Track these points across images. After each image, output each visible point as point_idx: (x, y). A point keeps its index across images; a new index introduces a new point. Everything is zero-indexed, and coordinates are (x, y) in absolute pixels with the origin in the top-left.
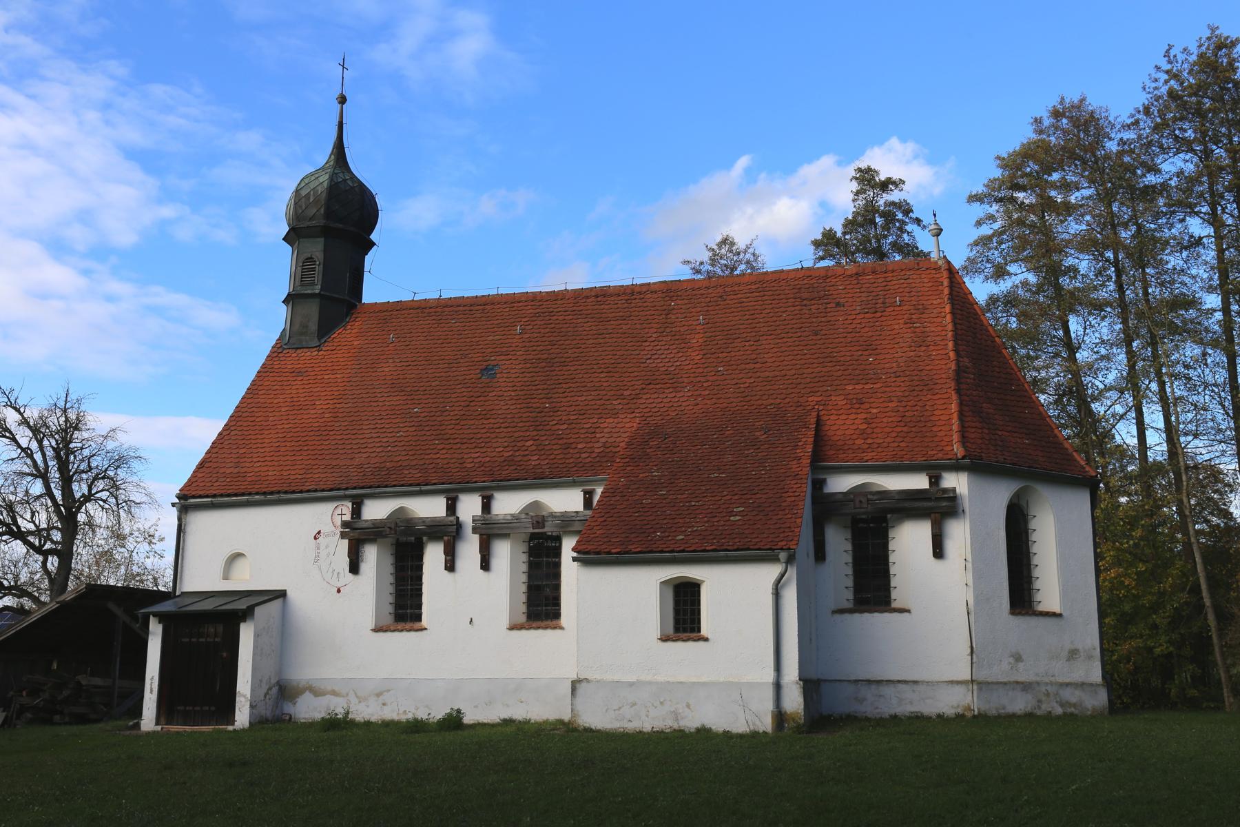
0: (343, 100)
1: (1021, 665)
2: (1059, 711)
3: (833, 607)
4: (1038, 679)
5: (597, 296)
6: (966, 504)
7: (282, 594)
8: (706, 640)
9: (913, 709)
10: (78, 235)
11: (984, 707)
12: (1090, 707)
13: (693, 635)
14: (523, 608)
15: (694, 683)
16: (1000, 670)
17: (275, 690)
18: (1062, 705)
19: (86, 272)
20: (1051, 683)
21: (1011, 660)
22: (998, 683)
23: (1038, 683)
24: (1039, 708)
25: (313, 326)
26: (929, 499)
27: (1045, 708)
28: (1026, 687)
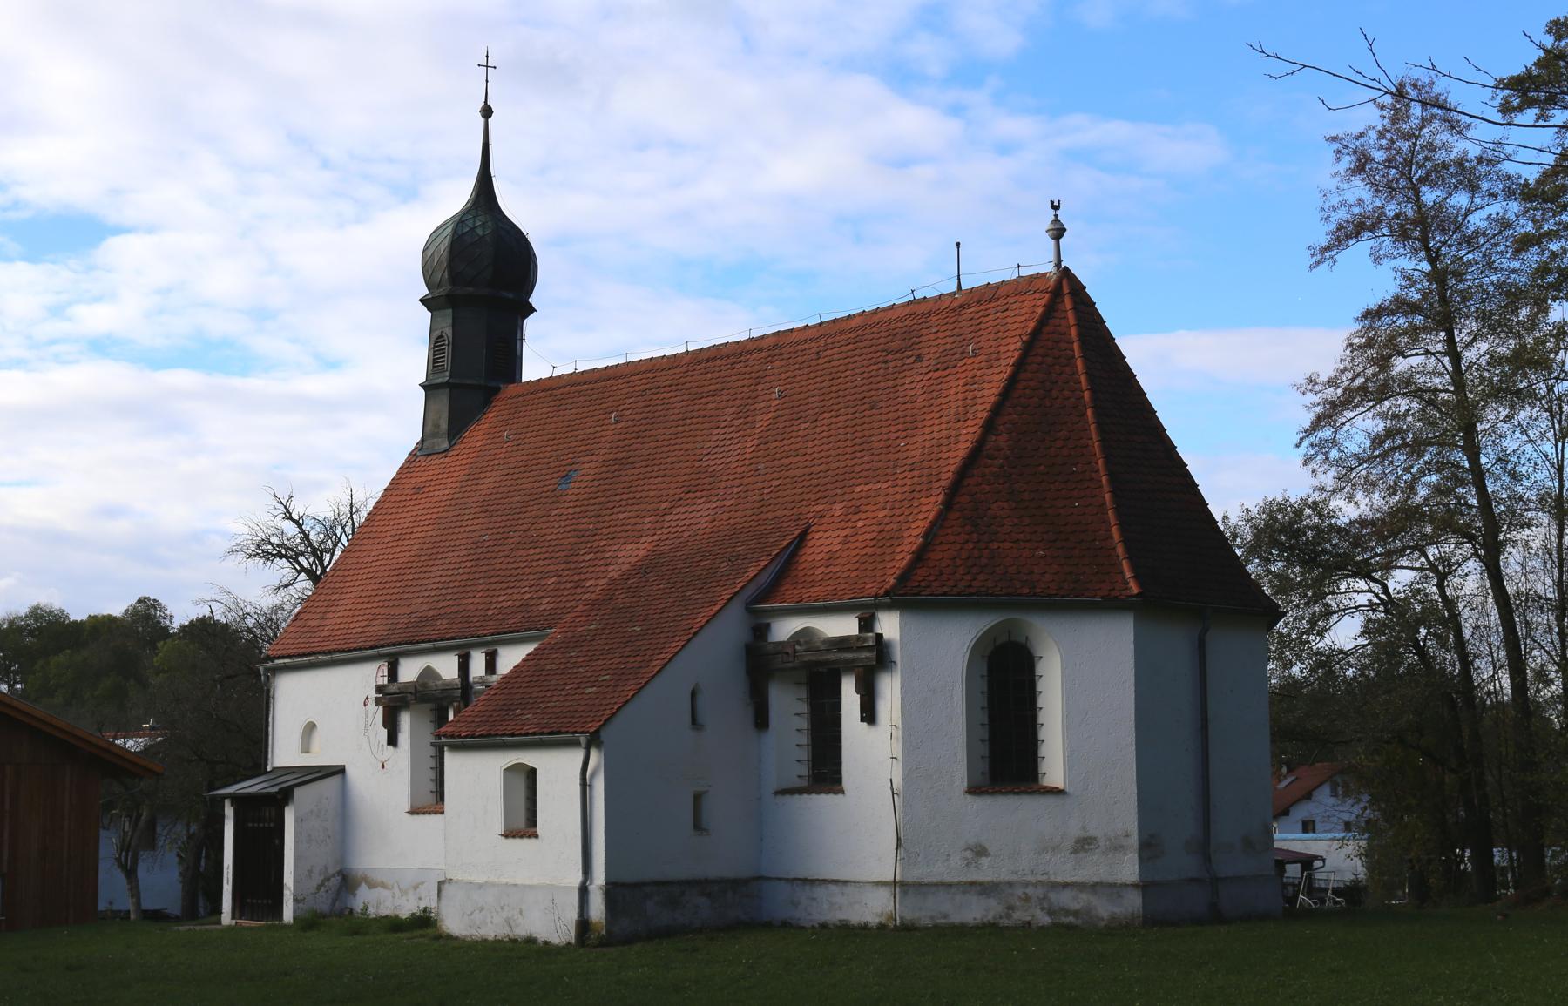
0: (487, 112)
1: (985, 861)
2: (1045, 920)
4: (1014, 878)
5: (708, 360)
6: (897, 655)
7: (340, 771)
10: (928, 51)
11: (909, 916)
15: (525, 886)
16: (950, 868)
17: (335, 881)
18: (1051, 913)
19: (956, 110)
20: (1035, 885)
21: (968, 854)
22: (936, 885)
23: (1010, 884)
24: (1009, 916)
25: (444, 426)
26: (849, 649)
27: (1020, 916)
28: (986, 889)
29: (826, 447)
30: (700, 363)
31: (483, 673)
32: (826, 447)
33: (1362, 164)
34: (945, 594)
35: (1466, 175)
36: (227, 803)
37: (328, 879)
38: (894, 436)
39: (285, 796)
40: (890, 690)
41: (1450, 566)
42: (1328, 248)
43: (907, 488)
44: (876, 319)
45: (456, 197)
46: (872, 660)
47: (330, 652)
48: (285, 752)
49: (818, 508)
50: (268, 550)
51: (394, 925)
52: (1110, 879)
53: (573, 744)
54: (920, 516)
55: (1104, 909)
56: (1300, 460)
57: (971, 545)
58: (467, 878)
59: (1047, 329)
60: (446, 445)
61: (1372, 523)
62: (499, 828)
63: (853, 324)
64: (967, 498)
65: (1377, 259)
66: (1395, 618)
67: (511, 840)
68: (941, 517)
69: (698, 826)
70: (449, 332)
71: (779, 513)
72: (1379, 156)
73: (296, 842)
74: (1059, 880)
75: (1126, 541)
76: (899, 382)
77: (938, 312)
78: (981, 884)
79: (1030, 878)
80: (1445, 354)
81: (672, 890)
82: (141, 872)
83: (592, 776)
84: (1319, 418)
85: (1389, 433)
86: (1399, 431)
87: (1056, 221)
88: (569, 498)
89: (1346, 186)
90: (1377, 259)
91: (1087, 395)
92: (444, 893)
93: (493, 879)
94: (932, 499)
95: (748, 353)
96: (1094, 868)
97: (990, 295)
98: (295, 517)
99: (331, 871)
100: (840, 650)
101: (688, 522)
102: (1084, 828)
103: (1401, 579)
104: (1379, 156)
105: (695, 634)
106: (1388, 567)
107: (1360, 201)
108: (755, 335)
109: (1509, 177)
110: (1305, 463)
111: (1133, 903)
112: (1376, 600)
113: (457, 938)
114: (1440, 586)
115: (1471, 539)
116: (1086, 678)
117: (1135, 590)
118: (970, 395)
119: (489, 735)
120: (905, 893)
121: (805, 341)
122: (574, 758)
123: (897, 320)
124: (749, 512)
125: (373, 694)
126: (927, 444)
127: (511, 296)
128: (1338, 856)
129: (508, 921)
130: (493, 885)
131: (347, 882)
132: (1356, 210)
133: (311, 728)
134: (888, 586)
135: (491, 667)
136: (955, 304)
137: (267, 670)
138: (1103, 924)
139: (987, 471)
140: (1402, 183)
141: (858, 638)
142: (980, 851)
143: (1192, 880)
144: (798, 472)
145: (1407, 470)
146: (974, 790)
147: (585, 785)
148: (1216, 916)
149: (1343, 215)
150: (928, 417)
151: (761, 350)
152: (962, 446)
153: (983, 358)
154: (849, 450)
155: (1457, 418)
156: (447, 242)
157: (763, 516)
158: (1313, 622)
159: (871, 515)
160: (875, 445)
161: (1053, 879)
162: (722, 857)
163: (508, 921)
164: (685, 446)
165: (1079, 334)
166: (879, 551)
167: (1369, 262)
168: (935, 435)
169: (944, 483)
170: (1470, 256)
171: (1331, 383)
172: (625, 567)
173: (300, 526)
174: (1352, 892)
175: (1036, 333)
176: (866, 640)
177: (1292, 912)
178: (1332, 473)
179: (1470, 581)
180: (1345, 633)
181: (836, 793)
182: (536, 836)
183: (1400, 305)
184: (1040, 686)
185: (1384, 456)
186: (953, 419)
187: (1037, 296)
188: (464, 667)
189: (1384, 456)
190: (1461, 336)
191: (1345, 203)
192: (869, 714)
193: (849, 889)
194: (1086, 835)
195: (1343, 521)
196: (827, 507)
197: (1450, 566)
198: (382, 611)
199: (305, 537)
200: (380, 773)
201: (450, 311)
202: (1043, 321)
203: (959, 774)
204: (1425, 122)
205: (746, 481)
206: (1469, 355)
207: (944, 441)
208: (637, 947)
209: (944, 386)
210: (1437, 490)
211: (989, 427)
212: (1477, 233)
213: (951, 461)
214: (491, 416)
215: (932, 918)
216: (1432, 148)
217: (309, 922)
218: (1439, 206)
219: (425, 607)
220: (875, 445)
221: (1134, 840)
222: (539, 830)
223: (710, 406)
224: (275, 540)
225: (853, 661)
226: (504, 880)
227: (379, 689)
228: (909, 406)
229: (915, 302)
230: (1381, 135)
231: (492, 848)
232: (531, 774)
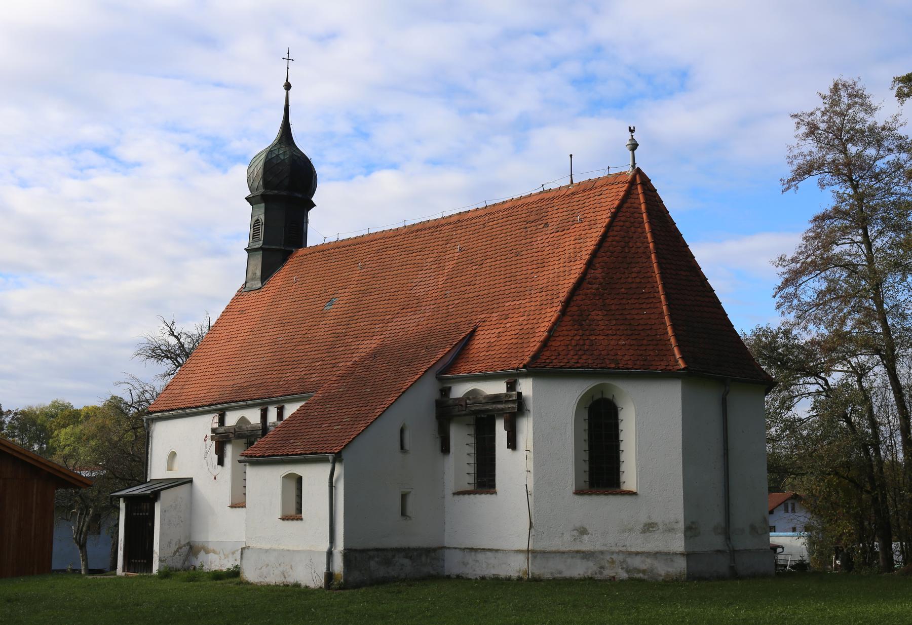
0: (288, 86)
1: (585, 537)
2: (624, 575)
3: (454, 491)
6: (530, 405)
7: (190, 481)
9: (495, 573)
12: (663, 573)
14: (586, 477)
16: (564, 542)
18: (628, 571)
20: (619, 553)
23: (602, 552)
24: (601, 573)
25: (259, 273)
26: (500, 402)
27: (608, 573)
28: (586, 555)
29: (488, 280)
30: (412, 232)
31: (275, 420)
32: (488, 280)
33: (813, 130)
34: (561, 367)
35: (875, 137)
36: (122, 500)
37: (181, 548)
38: (530, 272)
39: (154, 497)
40: (526, 428)
41: (864, 370)
42: (793, 180)
43: (538, 303)
44: (520, 203)
46: (515, 409)
47: (185, 408)
48: (158, 470)
49: (483, 316)
50: (158, 353)
51: (218, 576)
52: (666, 550)
53: (324, 460)
54: (547, 319)
55: (662, 569)
56: (774, 306)
57: (578, 338)
58: (259, 546)
59: (626, 205)
60: (260, 285)
61: (818, 343)
62: (279, 514)
63: (506, 206)
64: (575, 308)
65: (822, 186)
66: (832, 403)
67: (286, 522)
68: (559, 320)
69: (403, 513)
70: (262, 217)
71: (458, 320)
72: (823, 126)
73: (161, 524)
74: (633, 550)
75: (676, 336)
76: (534, 239)
77: (558, 197)
78: (583, 552)
79: (614, 549)
80: (862, 243)
81: (387, 555)
82: (89, 547)
83: (336, 481)
84: (787, 280)
85: (829, 290)
86: (834, 290)
87: (633, 139)
88: (331, 314)
89: (803, 143)
90: (822, 186)
91: (651, 245)
92: (244, 555)
93: (275, 546)
94: (554, 309)
95: (442, 225)
96: (655, 543)
97: (590, 187)
98: (176, 334)
99: (183, 543)
100: (495, 403)
101: (402, 327)
102: (649, 517)
103: (835, 378)
104: (823, 126)
105: (404, 392)
106: (828, 371)
107: (811, 153)
108: (446, 215)
109: (901, 138)
110: (778, 307)
111: (681, 565)
112: (821, 389)
113: (252, 584)
114: (859, 381)
115: (878, 352)
116: (653, 421)
118: (578, 246)
119: (273, 456)
120: (534, 557)
121: (476, 218)
122: (326, 469)
123: (533, 203)
124: (439, 320)
125: (210, 434)
126: (551, 276)
127: (300, 196)
128: (791, 543)
129: (283, 574)
130: (274, 550)
131: (193, 549)
132: (808, 158)
133: (173, 455)
134: (525, 362)
135: (280, 415)
136: (569, 192)
137: (147, 420)
138: (661, 578)
140: (836, 142)
141: (506, 395)
142: (583, 531)
143: (718, 551)
144: (471, 295)
145: (841, 310)
146: (579, 492)
147: (331, 486)
148: (735, 575)
149: (800, 161)
150: (551, 259)
151: (450, 224)
152: (572, 276)
153: (586, 223)
154: (502, 281)
155: (871, 281)
156: (262, 163)
157: (449, 322)
158: (783, 402)
159: (516, 320)
160: (518, 278)
161: (629, 549)
163: (283, 574)
164: (402, 282)
165: (647, 208)
166: (520, 341)
167: (817, 187)
168: (556, 270)
169: (560, 299)
170: (878, 185)
171: (794, 260)
172: (363, 354)
173: (179, 340)
174: (801, 566)
175: (619, 207)
176: (511, 396)
178: (793, 314)
179: (878, 375)
180: (802, 409)
181: (492, 494)
182: (302, 519)
183: (838, 212)
184: (622, 426)
185: (825, 303)
186: (567, 260)
187: (620, 185)
188: (264, 416)
189: (825, 303)
190: (872, 232)
191: (801, 154)
192: (512, 443)
193: (500, 555)
194: (651, 521)
195: (802, 342)
196: (488, 315)
197: (864, 370)
198: (217, 383)
199: (182, 346)
200: (212, 481)
201: (263, 204)
202: (624, 201)
203: (570, 483)
204: (849, 107)
205: (438, 301)
206: (878, 243)
207: (561, 274)
208: (363, 590)
209: (561, 241)
210: (860, 322)
211: (590, 264)
212: (883, 172)
213: (566, 286)
214: (287, 267)
215: (552, 573)
216: (854, 121)
217: (165, 574)
218: (859, 155)
219: (243, 381)
220: (518, 278)
221: (681, 525)
222: (303, 515)
223: (418, 257)
224: (163, 348)
225: (503, 409)
226: (281, 547)
227: (213, 430)
228: (540, 253)
229: (544, 192)
230: (823, 114)
231: (265, 524)
232: (299, 480)
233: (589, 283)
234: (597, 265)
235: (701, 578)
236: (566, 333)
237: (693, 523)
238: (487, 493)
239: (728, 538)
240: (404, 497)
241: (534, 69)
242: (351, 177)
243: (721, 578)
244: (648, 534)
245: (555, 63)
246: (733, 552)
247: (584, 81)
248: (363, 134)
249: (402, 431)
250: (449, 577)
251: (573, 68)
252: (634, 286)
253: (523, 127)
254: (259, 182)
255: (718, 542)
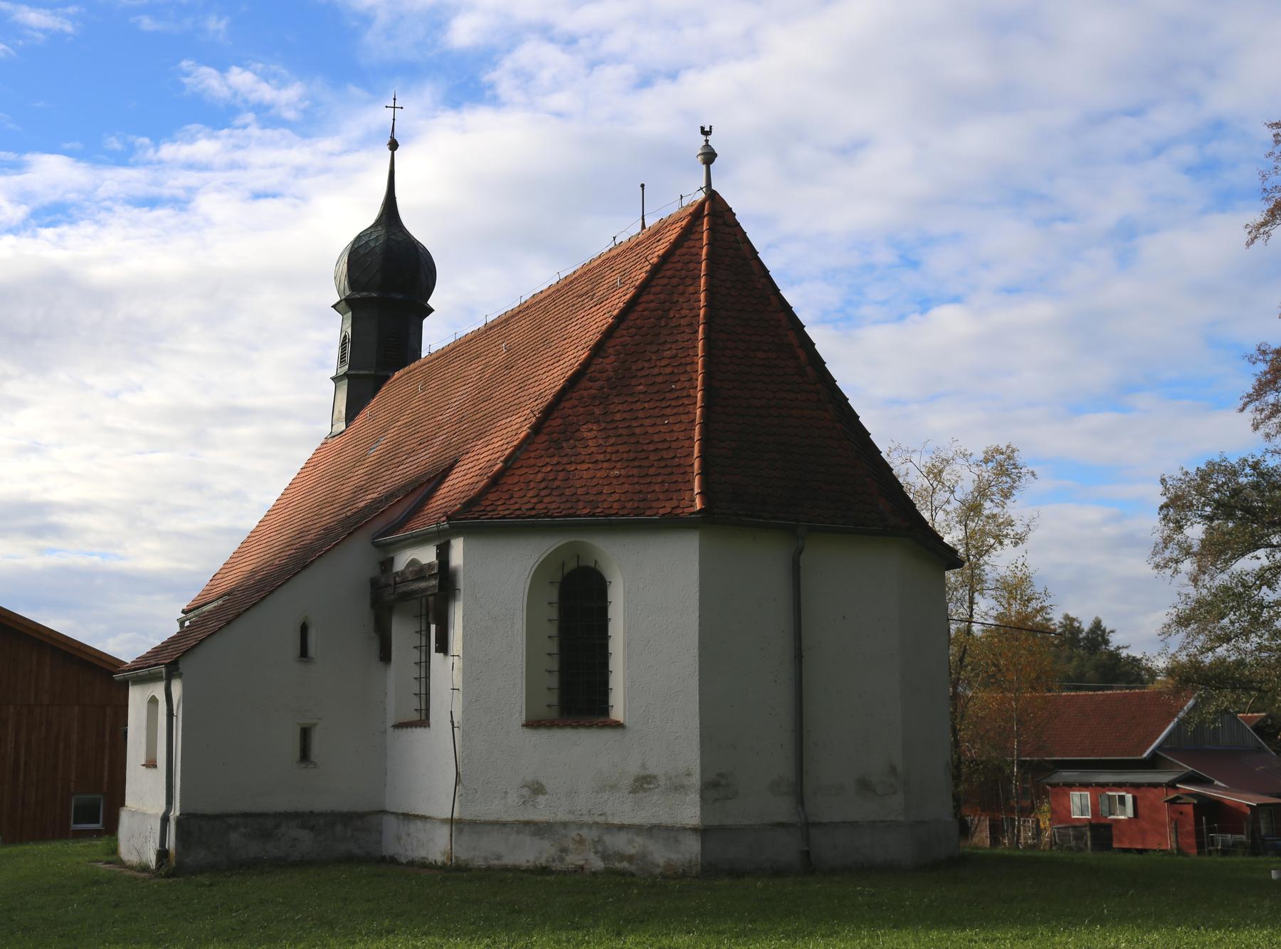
0: (709, 156)
1: (541, 799)
2: (598, 864)
4: (572, 818)
8: (618, 725)
12: (661, 862)
13: (602, 719)
18: (605, 857)
20: (590, 826)
21: (526, 792)
23: (565, 825)
24: (562, 860)
27: (573, 860)
34: (504, 517)
42: (1264, 224)
45: (366, 216)
55: (660, 854)
57: (549, 469)
69: (305, 755)
74: (617, 821)
78: (535, 824)
81: (263, 824)
87: (707, 145)
102: (643, 766)
111: (691, 848)
117: (698, 505)
120: (460, 831)
127: (400, 297)
138: (658, 871)
139: (585, 393)
142: (537, 789)
146: (533, 723)
148: (809, 866)
161: (611, 820)
162: (329, 790)
177: (809, 866)
193: (428, 825)
211: (598, 349)
215: (486, 859)
221: (696, 780)
233: (590, 380)
234: (611, 350)
235: (736, 872)
236: (532, 462)
237: (721, 775)
238: (590, 726)
239: (801, 801)
240: (305, 733)
241: (1131, 158)
242: (901, 317)
243: (778, 872)
244: (641, 795)
245: (1158, 149)
246: (808, 826)
247: (1203, 169)
248: (911, 263)
249: (304, 629)
250: (393, 861)
251: (1186, 153)
252: (660, 379)
253: (1126, 235)
254: (344, 282)
255: (782, 809)
